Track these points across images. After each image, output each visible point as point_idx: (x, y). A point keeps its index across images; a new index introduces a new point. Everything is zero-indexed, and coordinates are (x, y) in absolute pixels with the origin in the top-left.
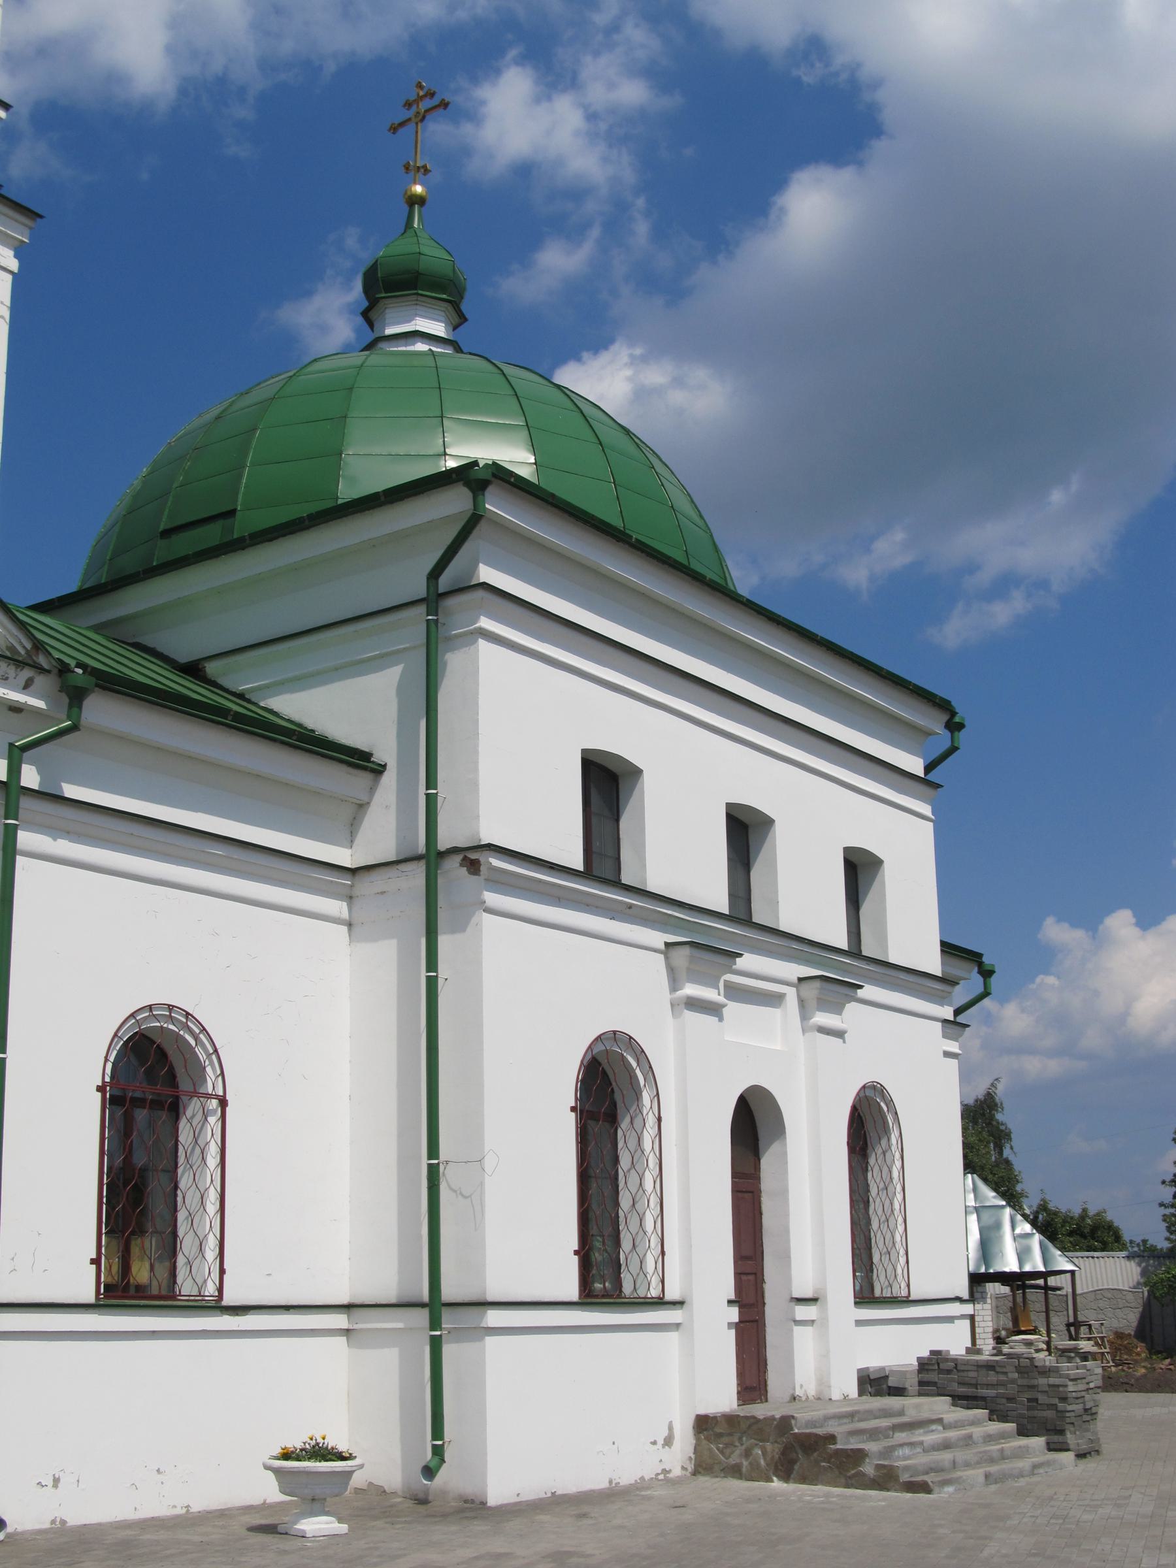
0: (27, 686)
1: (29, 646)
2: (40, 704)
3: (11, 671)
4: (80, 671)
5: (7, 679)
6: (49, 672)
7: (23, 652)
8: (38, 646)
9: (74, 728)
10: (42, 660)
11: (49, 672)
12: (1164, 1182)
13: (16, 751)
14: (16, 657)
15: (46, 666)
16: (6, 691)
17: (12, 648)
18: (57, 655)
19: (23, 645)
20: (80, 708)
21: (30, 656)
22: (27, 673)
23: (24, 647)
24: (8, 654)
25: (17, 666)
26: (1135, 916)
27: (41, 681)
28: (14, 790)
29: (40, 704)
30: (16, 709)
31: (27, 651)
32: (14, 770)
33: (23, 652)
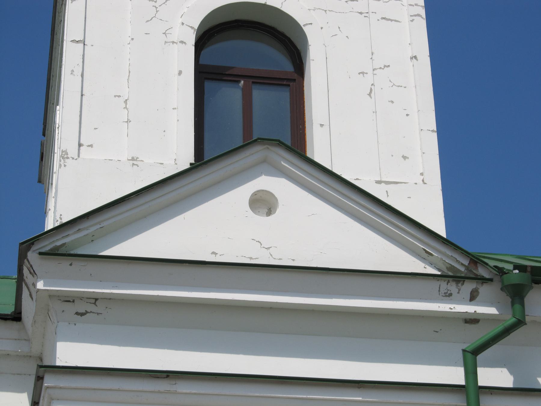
0: (473, 297)
1: (466, 262)
2: (492, 311)
3: (453, 287)
4: (517, 271)
5: (451, 295)
6: (491, 280)
7: (462, 269)
8: (475, 260)
9: (519, 323)
10: (482, 272)
11: (491, 280)
12: (378, 20)
13: (469, 356)
14: (459, 275)
15: (487, 276)
16: (452, 306)
17: (451, 268)
18: (492, 263)
19: (461, 264)
20: (523, 304)
21: (471, 271)
22: (468, 287)
23: (462, 264)
24: (450, 274)
25: (457, 282)
26: (511, 373)
27: (484, 290)
28: (472, 391)
29: (492, 311)
30: (472, 320)
31: (467, 268)
32: (471, 374)
33: (462, 269)
